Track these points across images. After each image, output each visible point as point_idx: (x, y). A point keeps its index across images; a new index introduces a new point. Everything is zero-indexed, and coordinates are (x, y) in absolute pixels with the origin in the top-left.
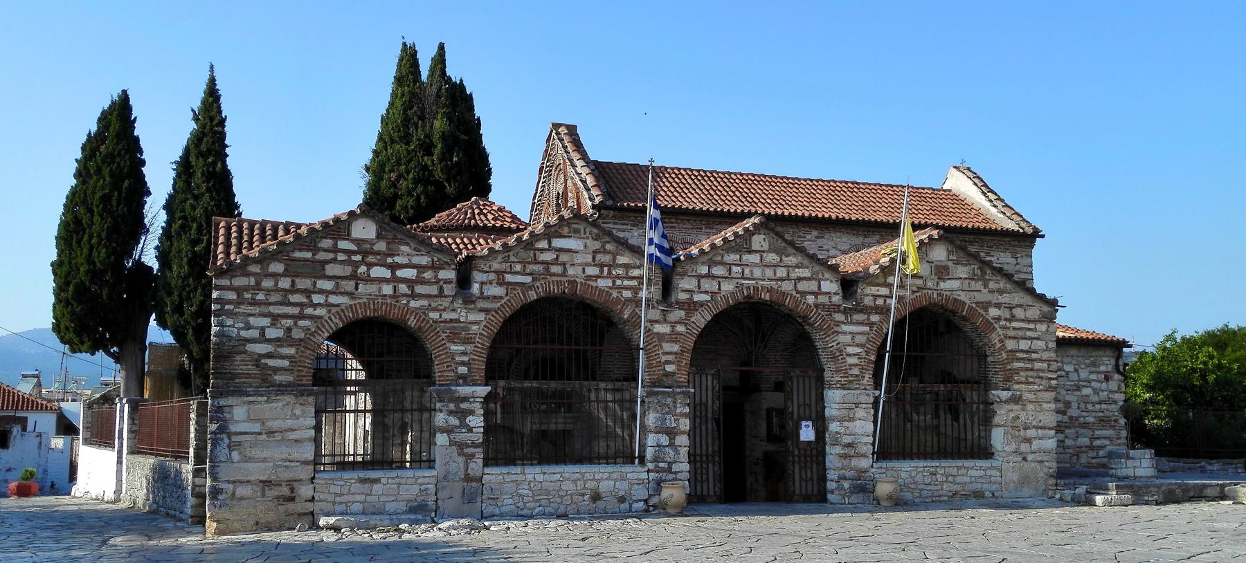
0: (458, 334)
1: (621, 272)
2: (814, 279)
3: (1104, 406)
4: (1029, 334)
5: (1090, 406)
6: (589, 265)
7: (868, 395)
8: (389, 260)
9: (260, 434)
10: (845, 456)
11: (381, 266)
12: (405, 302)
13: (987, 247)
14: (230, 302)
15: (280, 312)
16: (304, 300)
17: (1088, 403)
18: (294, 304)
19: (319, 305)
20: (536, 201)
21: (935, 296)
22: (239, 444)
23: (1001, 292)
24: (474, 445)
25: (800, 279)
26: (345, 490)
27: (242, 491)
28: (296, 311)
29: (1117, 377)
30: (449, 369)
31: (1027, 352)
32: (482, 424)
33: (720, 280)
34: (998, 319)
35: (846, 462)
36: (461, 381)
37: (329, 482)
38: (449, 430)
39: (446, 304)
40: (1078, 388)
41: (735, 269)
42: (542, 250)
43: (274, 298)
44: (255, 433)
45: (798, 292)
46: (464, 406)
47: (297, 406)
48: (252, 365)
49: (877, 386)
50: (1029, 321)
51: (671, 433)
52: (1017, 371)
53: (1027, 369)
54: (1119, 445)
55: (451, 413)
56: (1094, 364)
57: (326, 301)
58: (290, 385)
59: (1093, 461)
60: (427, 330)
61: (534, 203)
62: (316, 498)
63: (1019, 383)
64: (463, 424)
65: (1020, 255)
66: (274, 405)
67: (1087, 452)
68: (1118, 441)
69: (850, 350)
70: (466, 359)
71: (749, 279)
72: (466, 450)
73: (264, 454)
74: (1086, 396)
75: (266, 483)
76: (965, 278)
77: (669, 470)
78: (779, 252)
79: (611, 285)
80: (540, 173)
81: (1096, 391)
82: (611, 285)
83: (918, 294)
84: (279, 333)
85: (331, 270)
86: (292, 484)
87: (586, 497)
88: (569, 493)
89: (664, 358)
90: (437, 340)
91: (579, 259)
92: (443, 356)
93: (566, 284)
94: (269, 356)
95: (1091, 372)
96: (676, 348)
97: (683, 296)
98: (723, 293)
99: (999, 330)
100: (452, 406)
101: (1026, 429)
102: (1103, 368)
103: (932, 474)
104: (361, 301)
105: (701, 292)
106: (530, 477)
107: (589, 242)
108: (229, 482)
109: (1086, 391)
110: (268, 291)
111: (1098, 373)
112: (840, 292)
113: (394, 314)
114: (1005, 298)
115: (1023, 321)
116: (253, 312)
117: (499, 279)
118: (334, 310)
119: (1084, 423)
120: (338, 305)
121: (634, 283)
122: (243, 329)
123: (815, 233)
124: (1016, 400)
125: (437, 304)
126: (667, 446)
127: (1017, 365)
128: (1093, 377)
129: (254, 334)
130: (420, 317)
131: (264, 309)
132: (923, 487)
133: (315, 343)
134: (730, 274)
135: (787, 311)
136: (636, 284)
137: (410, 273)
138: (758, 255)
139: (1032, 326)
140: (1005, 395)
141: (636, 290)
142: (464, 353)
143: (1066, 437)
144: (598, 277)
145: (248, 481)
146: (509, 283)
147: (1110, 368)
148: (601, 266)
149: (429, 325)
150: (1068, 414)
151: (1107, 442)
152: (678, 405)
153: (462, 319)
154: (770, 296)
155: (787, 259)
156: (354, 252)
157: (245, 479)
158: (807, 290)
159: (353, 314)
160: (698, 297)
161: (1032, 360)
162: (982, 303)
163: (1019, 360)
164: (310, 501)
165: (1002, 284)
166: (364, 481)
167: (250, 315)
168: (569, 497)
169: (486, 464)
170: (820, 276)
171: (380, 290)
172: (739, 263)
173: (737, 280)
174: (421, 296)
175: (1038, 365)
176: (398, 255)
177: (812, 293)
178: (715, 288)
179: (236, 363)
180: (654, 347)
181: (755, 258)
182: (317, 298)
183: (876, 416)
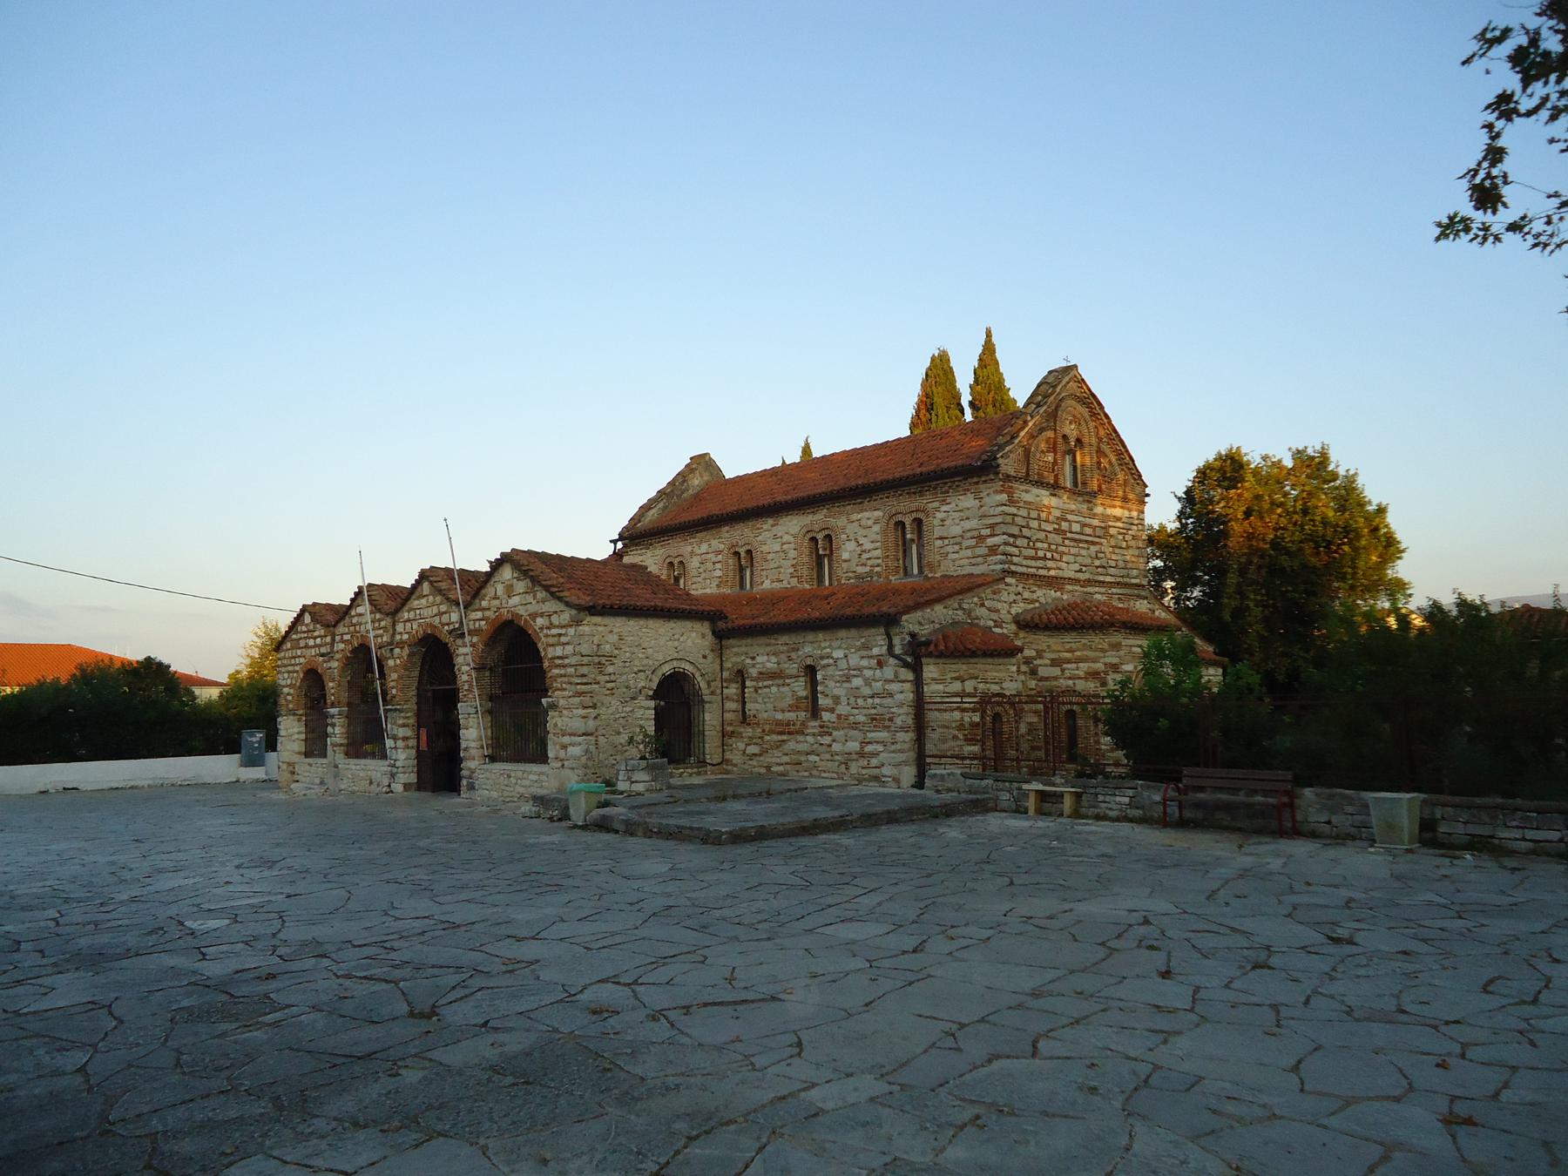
3: (877, 701)
5: (860, 701)
13: (942, 493)
17: (859, 697)
29: (892, 661)
40: (848, 679)
50: (563, 627)
53: (561, 676)
56: (866, 647)
59: (864, 772)
65: (985, 493)
67: (857, 760)
68: (893, 747)
74: (856, 688)
81: (868, 682)
95: (863, 657)
102: (876, 651)
109: (857, 682)
115: (558, 627)
119: (854, 723)
123: (770, 521)
128: (864, 663)
143: (834, 741)
150: (837, 712)
151: (880, 748)
161: (565, 666)
175: (571, 670)
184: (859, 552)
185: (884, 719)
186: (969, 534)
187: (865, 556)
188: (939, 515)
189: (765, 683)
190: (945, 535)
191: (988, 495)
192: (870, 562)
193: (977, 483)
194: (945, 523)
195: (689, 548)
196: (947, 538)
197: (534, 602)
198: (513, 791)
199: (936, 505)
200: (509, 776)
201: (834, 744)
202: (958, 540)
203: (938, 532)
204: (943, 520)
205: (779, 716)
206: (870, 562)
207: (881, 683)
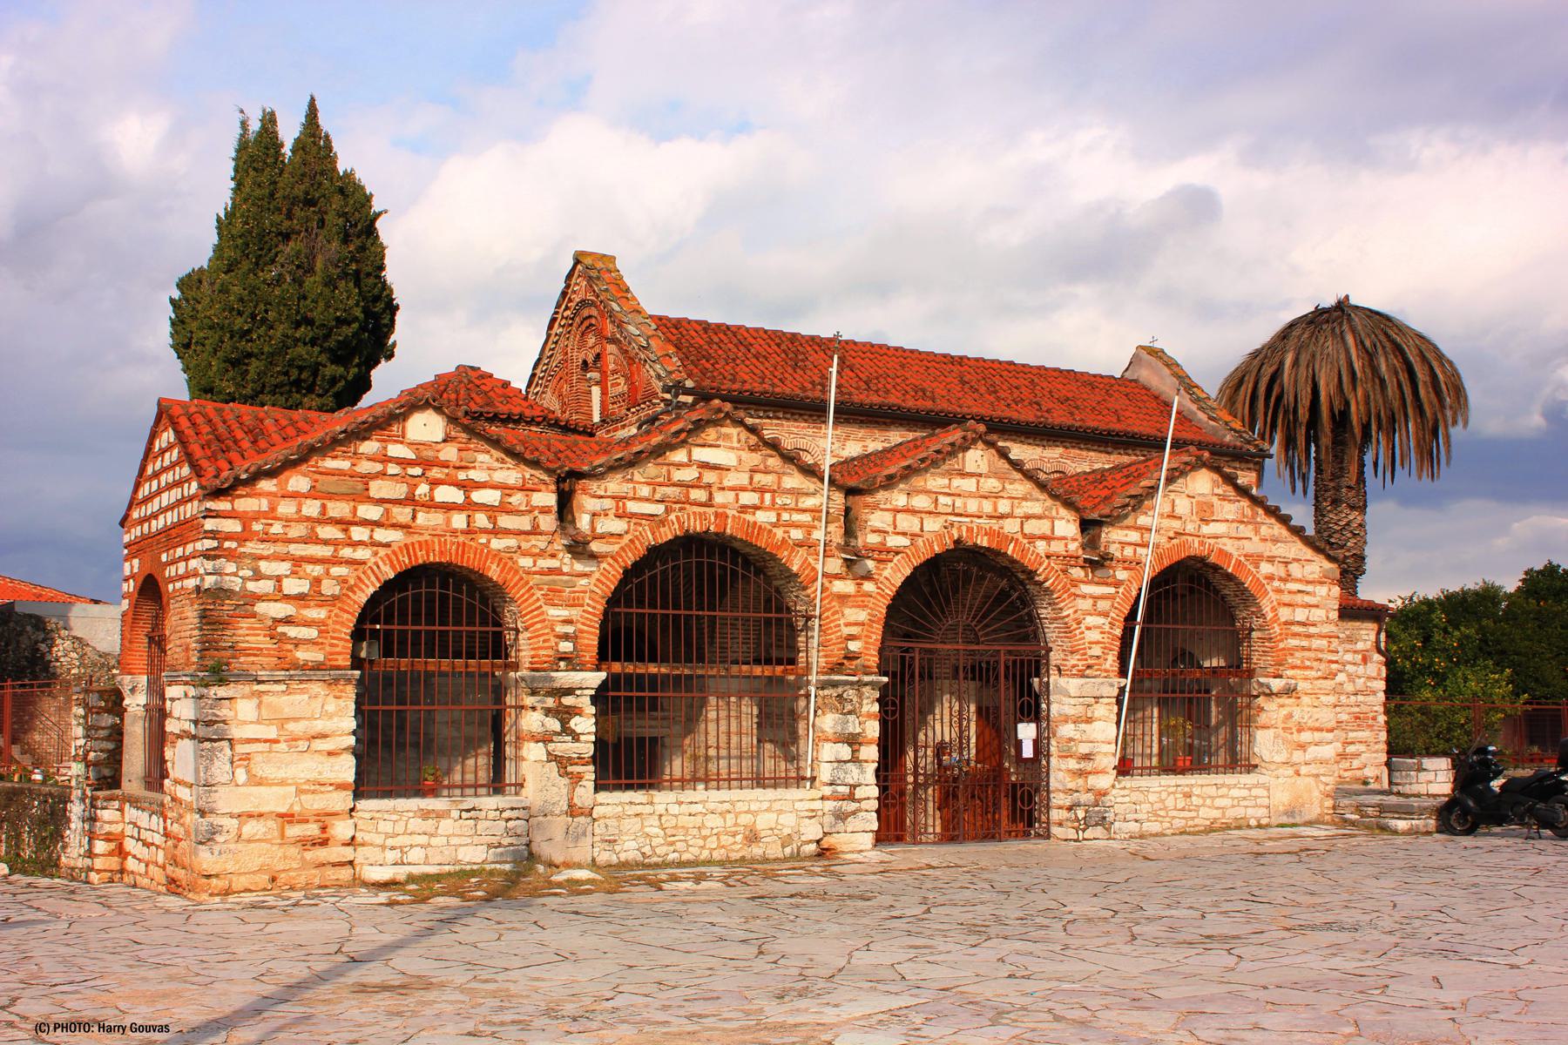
0: (560, 591)
1: (788, 500)
2: (1046, 517)
3: (1360, 698)
4: (1307, 599)
6: (743, 489)
7: (1112, 685)
8: (462, 476)
9: (276, 741)
10: (1081, 773)
11: (450, 485)
12: (483, 541)
14: (230, 537)
15: (303, 553)
16: (340, 535)
18: (326, 542)
19: (361, 543)
20: (538, 371)
21: (1196, 545)
22: (247, 757)
23: (1275, 541)
24: (580, 760)
25: (1028, 517)
26: (400, 828)
27: (250, 828)
28: (326, 552)
29: (1377, 657)
30: (546, 644)
31: (1304, 624)
32: (593, 729)
33: (923, 515)
34: (1271, 578)
35: (1080, 781)
36: (562, 664)
37: (378, 815)
38: (546, 738)
39: (543, 545)
41: (943, 500)
42: (679, 466)
43: (297, 531)
44: (266, 741)
45: (1025, 536)
46: (568, 701)
47: (331, 698)
48: (265, 636)
49: (1123, 673)
50: (1308, 582)
51: (853, 741)
52: (1291, 651)
53: (1303, 649)
54: (1376, 752)
55: (548, 712)
56: (1350, 640)
57: (371, 537)
58: (318, 667)
59: (1346, 774)
60: (516, 585)
61: (533, 375)
62: (359, 839)
63: (1293, 667)
64: (566, 730)
66: (298, 697)
69: (1090, 620)
70: (570, 629)
71: (961, 515)
72: (570, 769)
73: (281, 774)
75: (288, 818)
76: (1233, 521)
77: (851, 797)
78: (1001, 478)
79: (774, 520)
80: (550, 327)
82: (774, 520)
83: (1175, 541)
84: (302, 586)
85: (378, 489)
86: (324, 819)
87: (739, 838)
88: (715, 831)
89: (846, 631)
90: (530, 601)
91: (731, 479)
92: (539, 626)
93: (713, 518)
94: (288, 621)
96: (862, 616)
97: (873, 539)
98: (927, 536)
99: (1271, 593)
100: (550, 702)
101: (1299, 731)
102: (1360, 646)
103: (1188, 796)
104: (421, 538)
105: (898, 533)
106: (660, 809)
107: (745, 455)
108: (232, 816)
110: (288, 521)
111: (1355, 652)
112: (1079, 536)
113: (470, 561)
114: (1279, 550)
115: (1300, 581)
116: (266, 553)
117: (617, 508)
118: (382, 552)
120: (388, 545)
121: (806, 518)
122: (250, 579)
124: (1289, 691)
125: (530, 544)
126: (849, 761)
127: (1293, 642)
128: (1349, 657)
129: (265, 586)
130: (506, 564)
131: (280, 548)
132: (1175, 813)
133: (355, 602)
134: (936, 508)
135: (1006, 563)
136: (810, 519)
137: (490, 497)
138: (974, 480)
139: (1309, 588)
140: (1276, 684)
141: (809, 528)
142: (568, 622)
144: (756, 508)
145: (261, 815)
146: (633, 515)
147: (1369, 645)
148: (762, 491)
149: (517, 578)
151: (1362, 748)
152: (865, 702)
153: (566, 569)
154: (989, 542)
155: (1011, 487)
156: (412, 463)
157: (255, 810)
158: (1037, 532)
159: (410, 559)
160: (894, 541)
161: (1309, 636)
162: (1252, 556)
163: (1295, 635)
164: (349, 845)
165: (1278, 530)
166: (425, 815)
167: (261, 558)
168: (715, 838)
169: (597, 789)
170: (1054, 513)
171: (448, 521)
172: (947, 490)
173: (945, 517)
174: (507, 532)
175: (1316, 643)
176: (474, 468)
177: (1043, 538)
178: (917, 529)
179: (240, 632)
180: (833, 614)
181: (969, 485)
182: (358, 533)
183: (1119, 715)
185: (1368, 718)
197: (1256, 539)
198: (1197, 817)
200: (1188, 796)
207: (1362, 680)
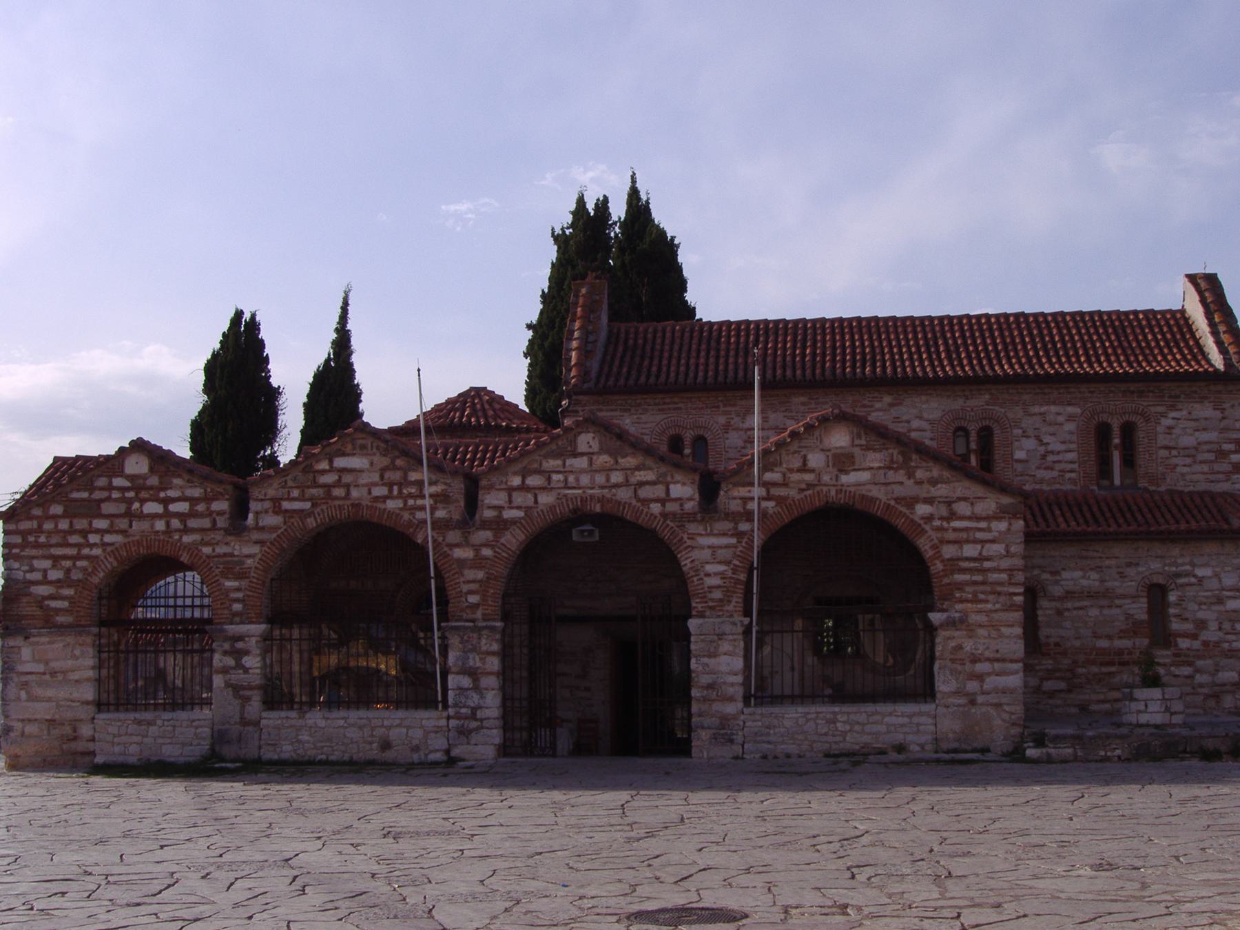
123: (888, 399)
184: (1042, 452)
186: (1205, 447)
187: (1050, 458)
188: (1167, 422)
189: (1077, 604)
190: (1172, 444)
191: (1233, 406)
192: (1058, 466)
193: (1220, 392)
194: (1174, 431)
195: (722, 420)
196: (1174, 448)
199: (1160, 409)
201: (1198, 676)
202: (1193, 452)
203: (1162, 440)
204: (1170, 428)
205: (1103, 643)
206: (1058, 467)
